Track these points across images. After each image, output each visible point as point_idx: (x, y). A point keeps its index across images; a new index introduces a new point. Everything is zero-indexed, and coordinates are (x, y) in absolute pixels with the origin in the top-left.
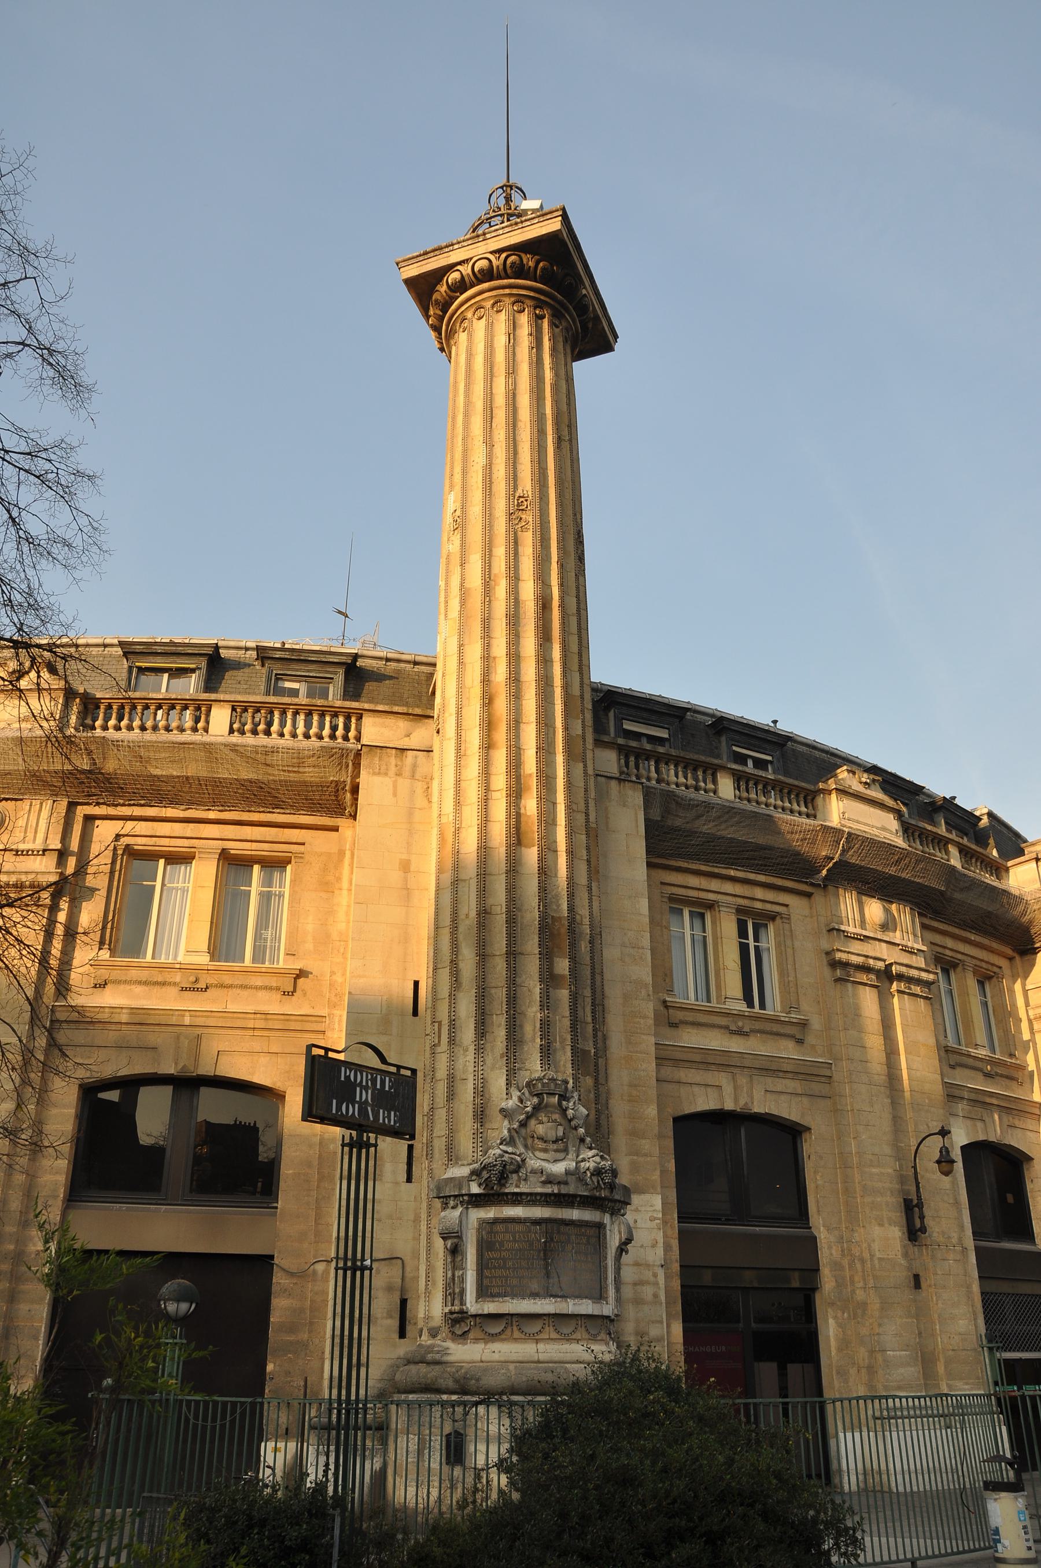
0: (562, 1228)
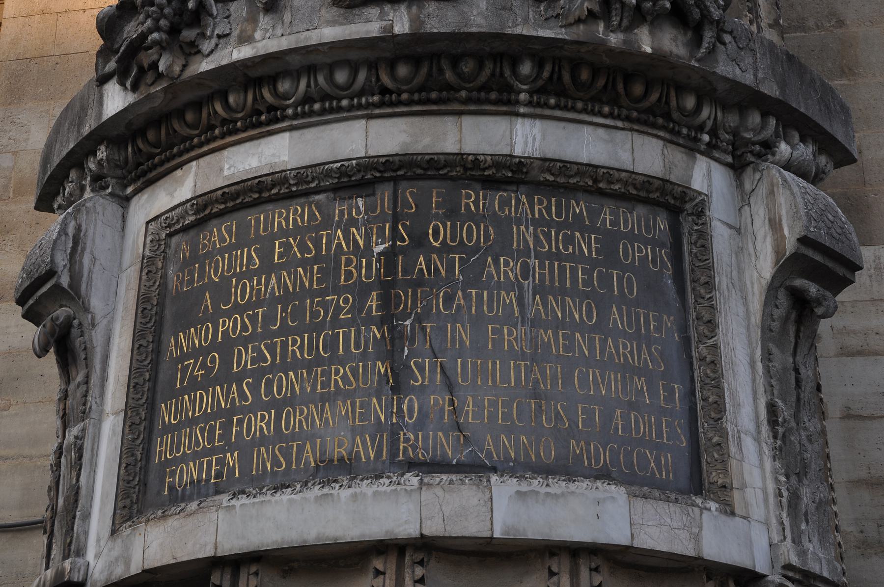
0: (471, 199)
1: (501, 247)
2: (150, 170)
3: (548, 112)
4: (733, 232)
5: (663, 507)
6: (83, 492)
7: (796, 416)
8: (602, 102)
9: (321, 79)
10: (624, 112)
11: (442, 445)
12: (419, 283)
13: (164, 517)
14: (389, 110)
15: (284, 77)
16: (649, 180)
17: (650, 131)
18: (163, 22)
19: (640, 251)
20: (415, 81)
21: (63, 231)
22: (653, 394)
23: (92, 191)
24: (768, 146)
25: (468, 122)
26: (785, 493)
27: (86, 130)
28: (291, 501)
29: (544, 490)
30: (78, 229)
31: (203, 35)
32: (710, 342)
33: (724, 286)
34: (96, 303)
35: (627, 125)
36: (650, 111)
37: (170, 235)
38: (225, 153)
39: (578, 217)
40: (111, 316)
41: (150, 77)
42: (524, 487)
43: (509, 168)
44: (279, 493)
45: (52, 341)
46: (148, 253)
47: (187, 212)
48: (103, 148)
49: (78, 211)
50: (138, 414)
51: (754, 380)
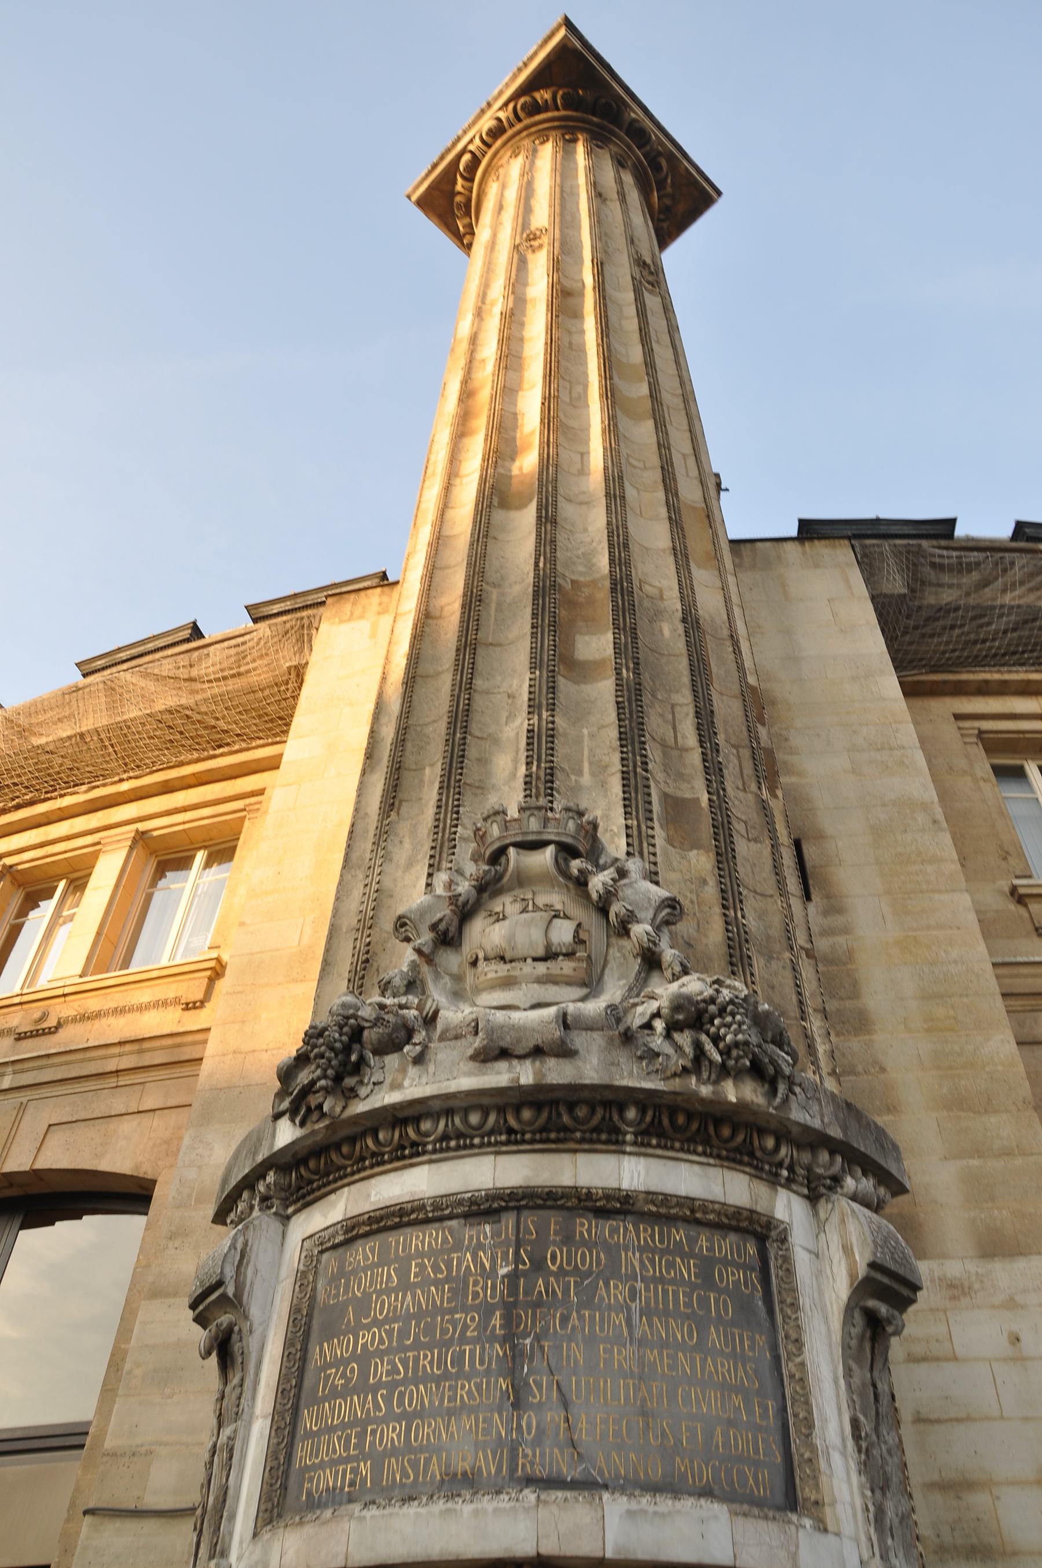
0: (584, 1226)
1: (612, 1271)
2: (309, 1194)
3: (650, 1151)
4: (813, 1256)
5: (762, 1525)
6: (231, 1492)
7: (877, 1429)
8: (696, 1142)
9: (457, 1121)
10: (715, 1151)
11: (558, 1462)
12: (538, 1304)
13: (301, 1523)
14: (514, 1148)
15: (426, 1118)
16: (738, 1211)
17: (738, 1167)
18: (330, 1072)
19: (733, 1274)
20: (537, 1124)
21: (233, 1246)
22: (750, 1411)
23: (260, 1210)
24: (837, 1180)
25: (581, 1158)
26: (871, 1508)
27: (260, 1158)
28: (417, 1515)
29: (651, 1509)
30: (246, 1244)
31: (361, 1082)
32: (798, 1360)
33: (807, 1307)
34: (255, 1311)
35: (718, 1162)
36: (737, 1150)
37: (321, 1252)
38: (373, 1181)
39: (679, 1244)
40: (266, 1324)
41: (315, 1116)
42: (634, 1506)
43: (618, 1200)
44: (406, 1506)
45: (215, 1345)
46: (301, 1267)
47: (337, 1232)
48: (272, 1173)
49: (246, 1227)
50: (283, 1418)
51: (838, 1396)
